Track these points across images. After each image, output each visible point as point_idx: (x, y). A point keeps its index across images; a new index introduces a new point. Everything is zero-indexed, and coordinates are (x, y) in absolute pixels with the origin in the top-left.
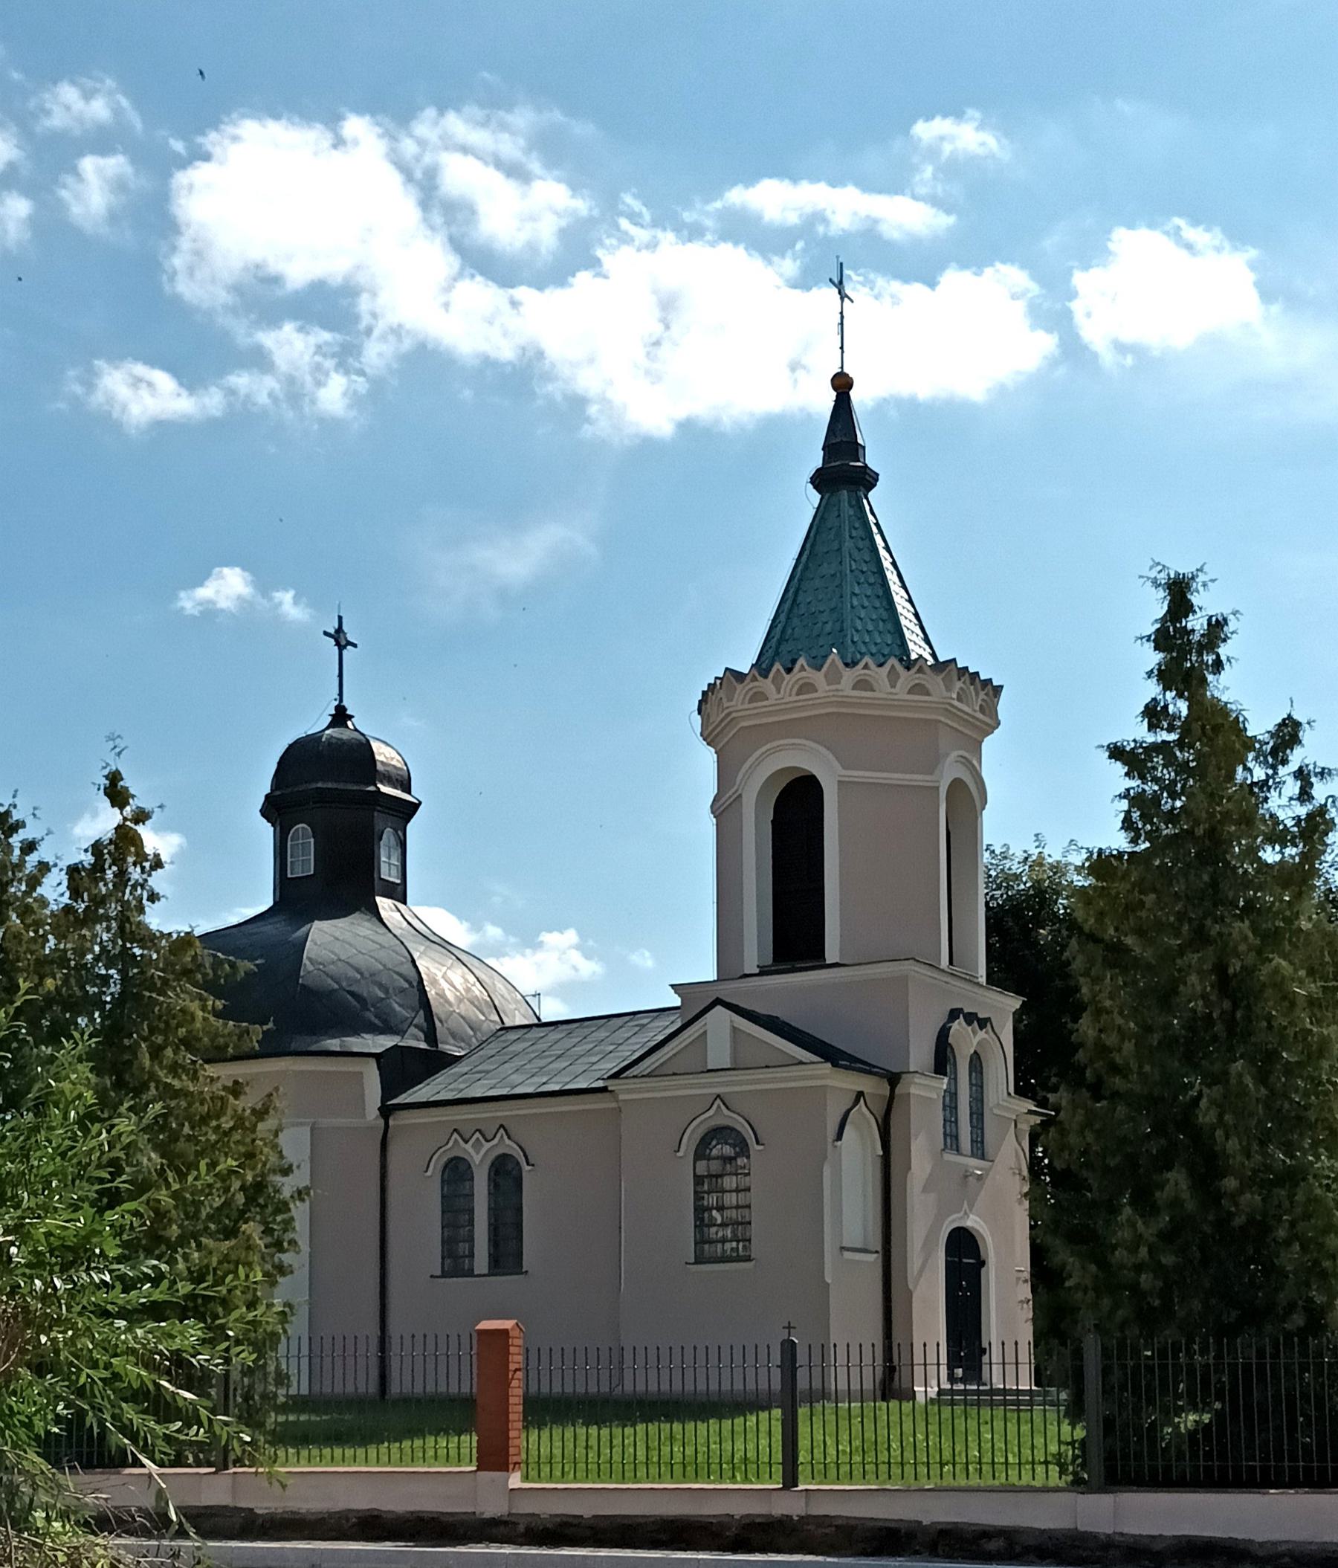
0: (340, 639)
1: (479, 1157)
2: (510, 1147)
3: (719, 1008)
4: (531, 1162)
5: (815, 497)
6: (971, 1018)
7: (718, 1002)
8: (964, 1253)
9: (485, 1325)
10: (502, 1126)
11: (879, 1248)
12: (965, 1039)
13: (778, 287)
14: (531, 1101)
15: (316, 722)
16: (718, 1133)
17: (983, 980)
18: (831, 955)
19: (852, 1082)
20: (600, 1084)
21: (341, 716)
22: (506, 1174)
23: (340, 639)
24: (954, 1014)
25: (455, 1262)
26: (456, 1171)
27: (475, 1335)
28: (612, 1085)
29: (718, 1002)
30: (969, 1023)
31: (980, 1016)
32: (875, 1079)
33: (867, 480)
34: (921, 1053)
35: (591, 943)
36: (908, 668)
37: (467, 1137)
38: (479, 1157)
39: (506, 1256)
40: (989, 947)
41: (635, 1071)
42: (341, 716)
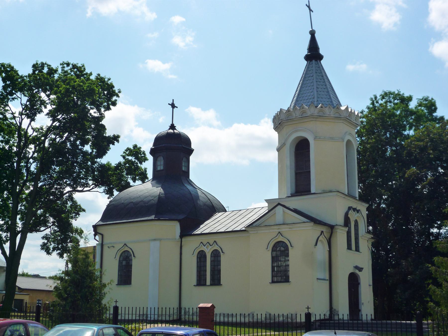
0: (173, 106)
1: (208, 251)
2: (216, 247)
3: (279, 207)
4: (292, 246)
5: (306, 62)
6: (355, 210)
7: (279, 204)
8: (354, 281)
9: (201, 305)
10: (201, 242)
11: (328, 279)
12: (353, 216)
13: (370, 285)
14: (215, 235)
15: (164, 129)
16: (279, 243)
17: (358, 198)
18: (313, 191)
19: (320, 228)
20: (244, 229)
21: (172, 127)
22: (216, 255)
23: (173, 106)
24: (350, 208)
25: (201, 282)
26: (201, 256)
27: (198, 309)
28: (248, 229)
29: (279, 204)
30: (354, 211)
31: (357, 209)
32: (327, 227)
33: (321, 57)
34: (340, 220)
35: (8, 83)
36: (334, 108)
37: (205, 244)
38: (208, 251)
39: (216, 281)
40: (358, 177)
41: (255, 224)
42: (172, 127)
